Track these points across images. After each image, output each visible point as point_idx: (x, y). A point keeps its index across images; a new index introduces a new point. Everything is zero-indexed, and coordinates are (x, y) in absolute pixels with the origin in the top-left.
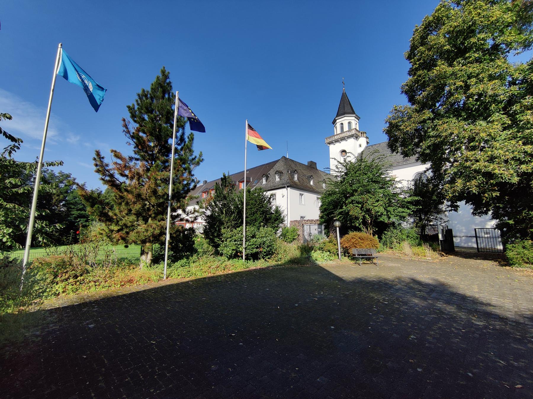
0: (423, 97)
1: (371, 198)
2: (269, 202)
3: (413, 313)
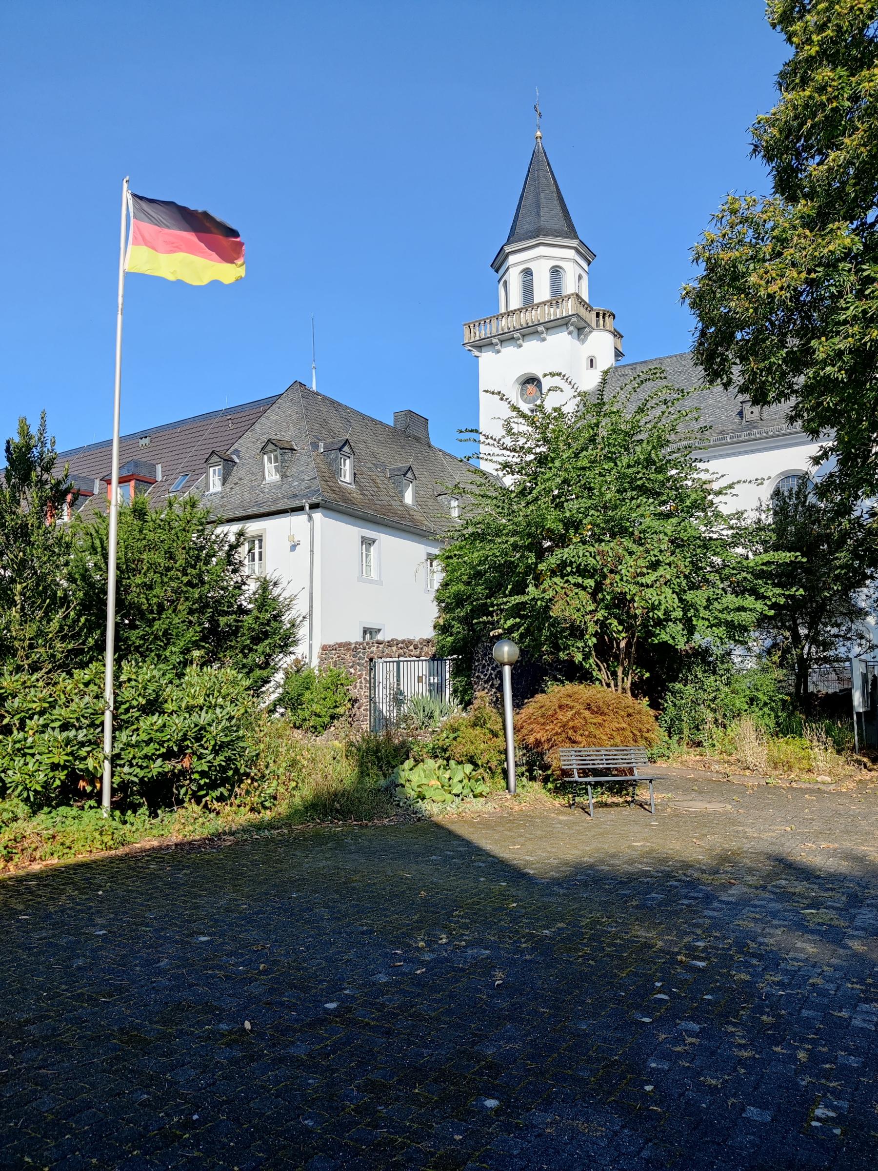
0: (830, 170)
1: (631, 553)
2: (230, 563)
3: (805, 1002)
